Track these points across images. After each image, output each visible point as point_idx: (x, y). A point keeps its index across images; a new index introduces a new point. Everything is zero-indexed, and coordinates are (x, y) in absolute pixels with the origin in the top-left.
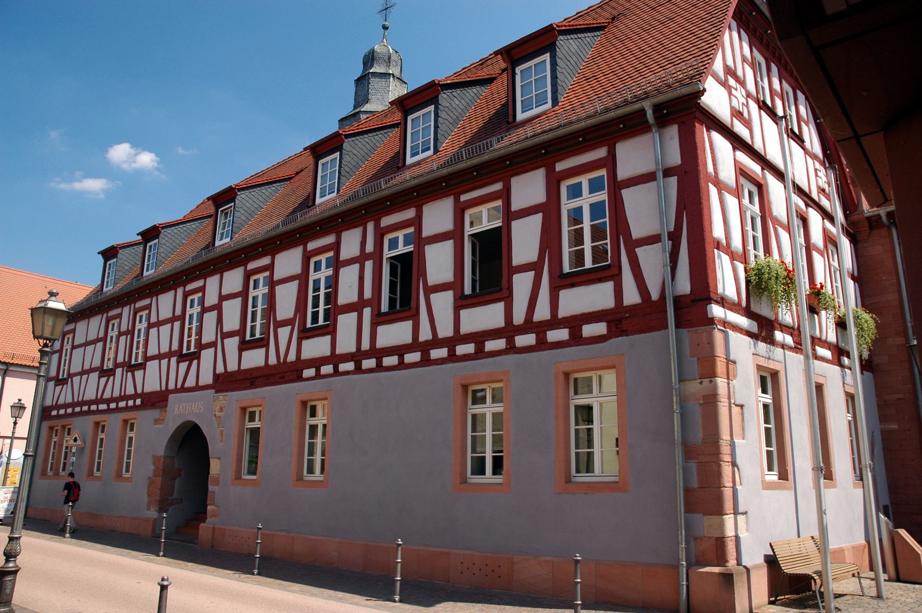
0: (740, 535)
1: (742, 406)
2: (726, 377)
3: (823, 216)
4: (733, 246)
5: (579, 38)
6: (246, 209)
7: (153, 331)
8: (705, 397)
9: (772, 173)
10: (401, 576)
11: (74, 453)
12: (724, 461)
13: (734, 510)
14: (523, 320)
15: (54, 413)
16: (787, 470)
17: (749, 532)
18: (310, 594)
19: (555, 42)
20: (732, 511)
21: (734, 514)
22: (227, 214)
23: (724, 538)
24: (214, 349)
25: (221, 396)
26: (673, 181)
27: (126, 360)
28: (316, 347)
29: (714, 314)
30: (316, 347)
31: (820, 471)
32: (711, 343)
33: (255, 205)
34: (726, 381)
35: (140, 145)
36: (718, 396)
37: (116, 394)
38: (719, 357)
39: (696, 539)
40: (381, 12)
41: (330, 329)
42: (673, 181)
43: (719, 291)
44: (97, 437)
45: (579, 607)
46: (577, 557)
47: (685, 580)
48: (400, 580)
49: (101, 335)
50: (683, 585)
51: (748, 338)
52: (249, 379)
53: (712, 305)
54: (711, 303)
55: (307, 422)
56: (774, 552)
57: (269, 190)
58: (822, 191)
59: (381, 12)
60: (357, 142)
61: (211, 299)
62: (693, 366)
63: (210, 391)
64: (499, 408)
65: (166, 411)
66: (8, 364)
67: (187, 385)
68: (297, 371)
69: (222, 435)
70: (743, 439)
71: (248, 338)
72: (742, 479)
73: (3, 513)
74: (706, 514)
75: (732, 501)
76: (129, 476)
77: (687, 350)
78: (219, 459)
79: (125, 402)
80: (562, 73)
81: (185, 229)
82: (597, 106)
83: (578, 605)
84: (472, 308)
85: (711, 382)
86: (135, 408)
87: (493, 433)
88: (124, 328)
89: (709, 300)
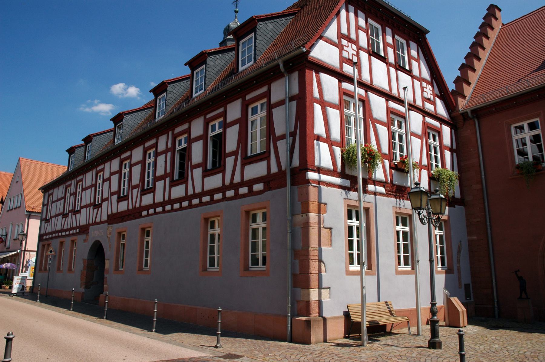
0: (323, 300)
1: (331, 229)
2: (317, 212)
3: (423, 114)
4: (332, 138)
5: (288, 19)
6: (129, 125)
7: (84, 192)
8: (304, 224)
9: (375, 93)
10: (157, 319)
11: (51, 258)
12: (311, 259)
13: (318, 286)
14: (229, 183)
15: (44, 237)
16: (371, 264)
17: (331, 299)
18: (118, 328)
19: (256, 26)
20: (317, 287)
21: (318, 288)
22: (120, 127)
23: (310, 301)
25: (110, 226)
26: (294, 103)
27: (73, 208)
28: (147, 199)
29: (309, 177)
30: (147, 199)
31: (363, 265)
32: (307, 194)
33: (135, 122)
34: (317, 214)
35: (129, 83)
36: (309, 223)
37: (69, 227)
38: (312, 201)
39: (298, 301)
40: (234, 3)
41: (152, 190)
42: (294, 103)
43: (315, 164)
45: (219, 335)
46: (219, 309)
47: (289, 324)
48: (156, 321)
49: (63, 195)
50: (289, 326)
51: (340, 190)
52: (121, 217)
53: (308, 172)
54: (308, 172)
55: (145, 239)
56: (348, 310)
57: (143, 113)
58: (425, 100)
59: (234, 3)
60: (176, 86)
61: (107, 175)
62: (298, 206)
63: (105, 224)
65: (88, 235)
66: (31, 212)
67: (97, 221)
68: (140, 212)
69: (110, 247)
70: (331, 247)
71: (122, 195)
72: (326, 270)
73: (17, 290)
74: (302, 288)
75: (317, 282)
76: (148, 269)
77: (296, 198)
78: (109, 260)
79: (72, 231)
80: (261, 43)
81: (106, 136)
82: (263, 62)
83: (219, 334)
84: (213, 175)
85: (306, 215)
86: (76, 234)
88: (72, 192)
89: (306, 170)
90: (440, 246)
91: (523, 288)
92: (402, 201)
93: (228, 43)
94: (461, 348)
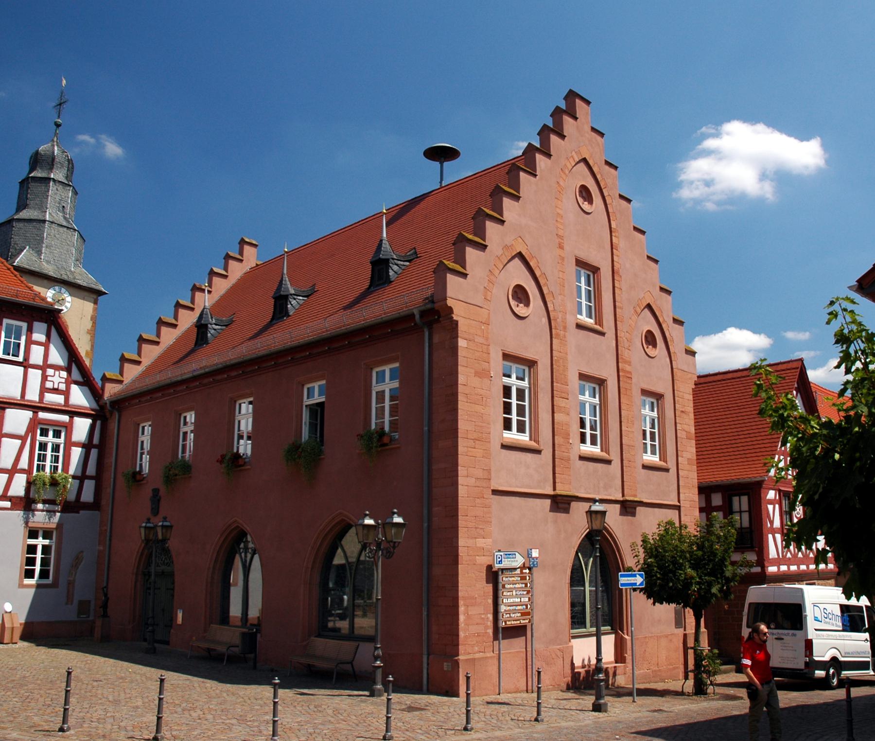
44: (179, 431)
59: (66, 102)
87: (391, 419)
90: (42, 558)
93: (32, 184)
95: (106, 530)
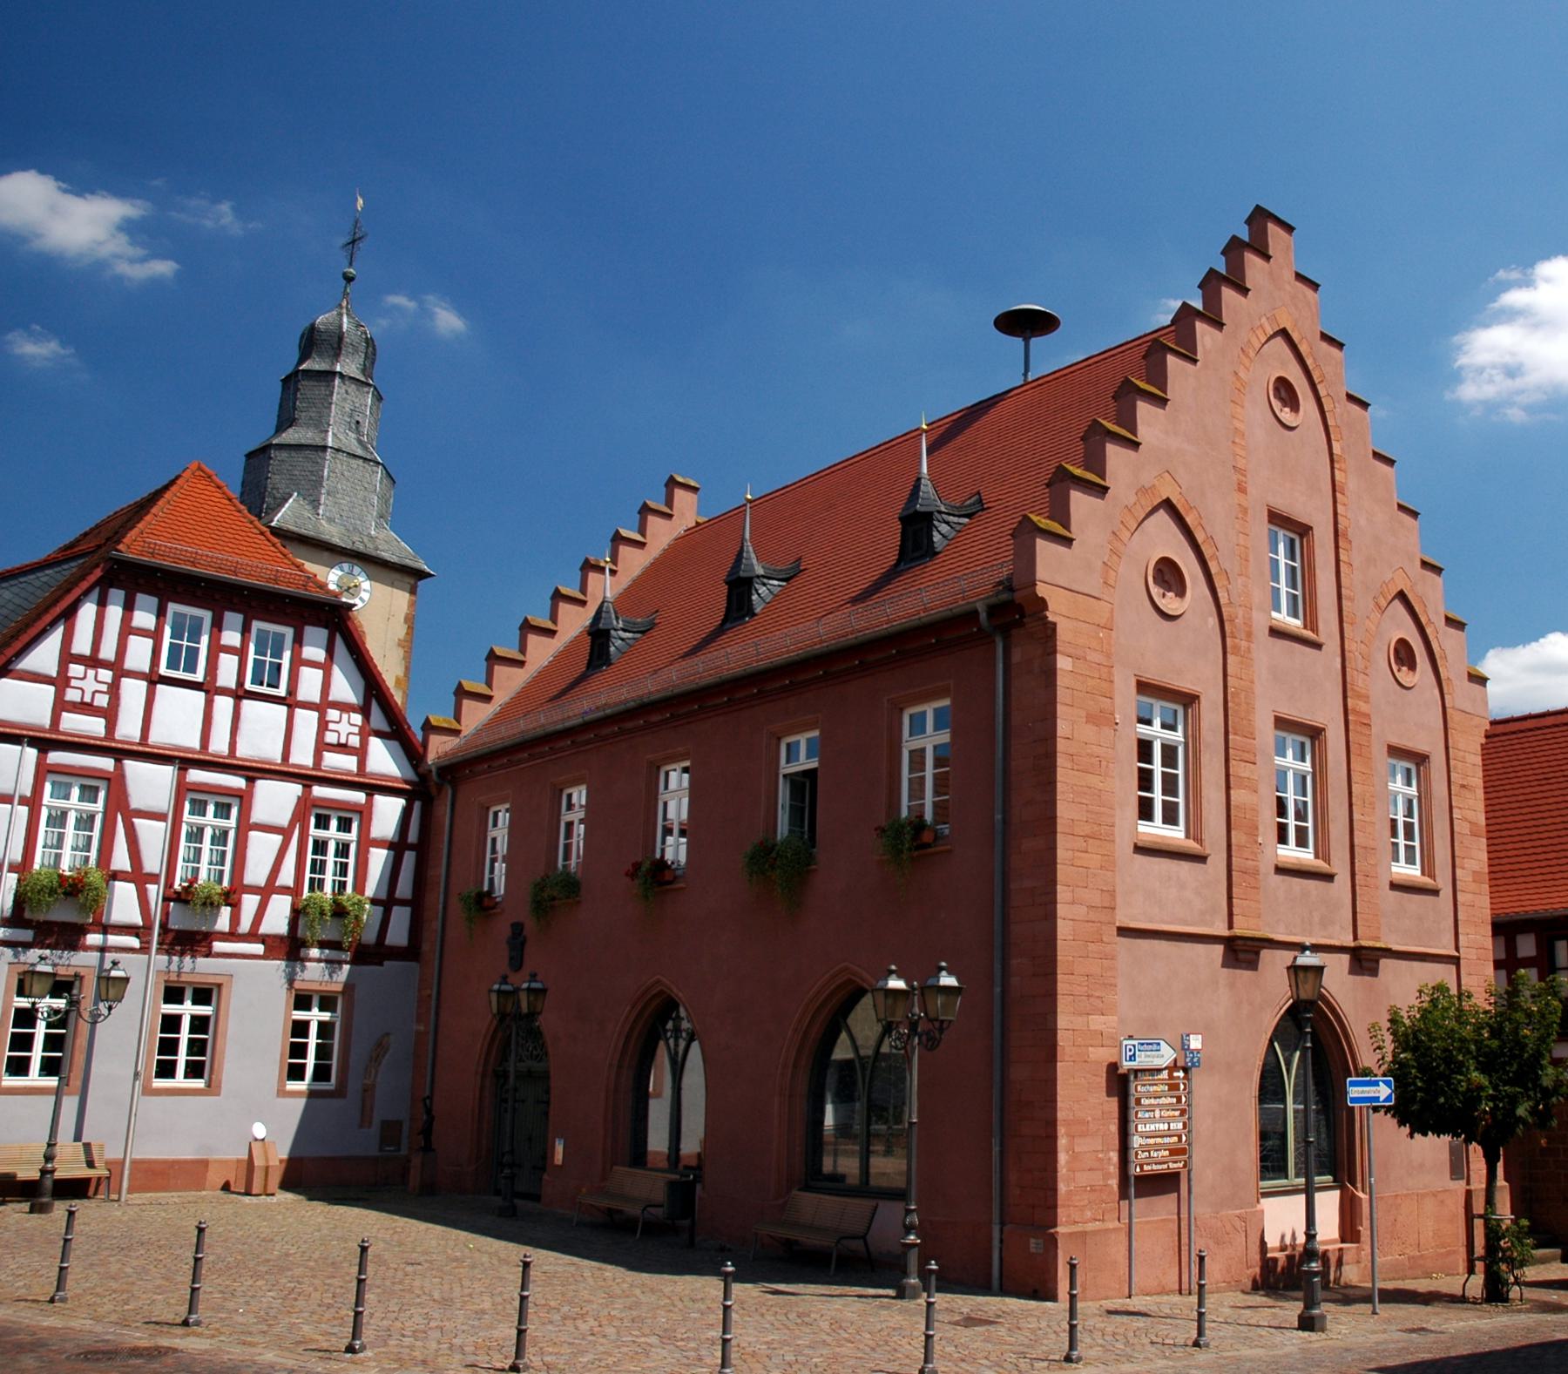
24: (1176, 1194)
64: (326, 1016)
91: (1049, 1208)
92: (188, 959)
94: (359, 1300)
95: (430, 996)
